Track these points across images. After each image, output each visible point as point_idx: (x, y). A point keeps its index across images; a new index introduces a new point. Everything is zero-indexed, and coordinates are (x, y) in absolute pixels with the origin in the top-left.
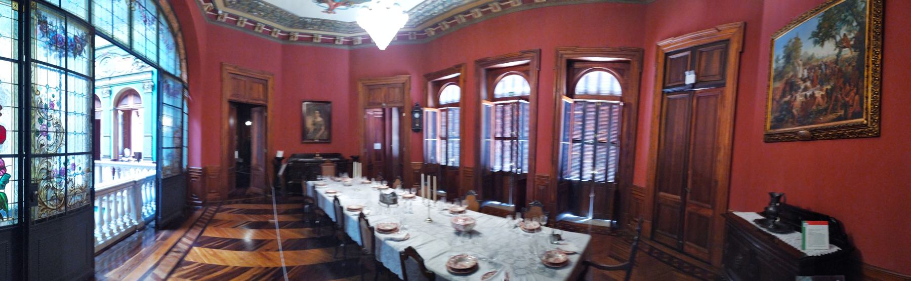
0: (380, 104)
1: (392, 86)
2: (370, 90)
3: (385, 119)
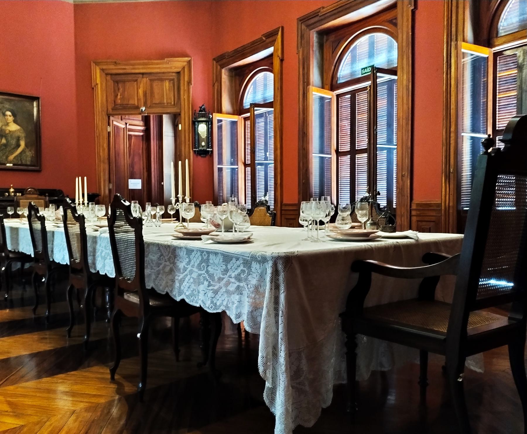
0: (138, 108)
1: (159, 77)
2: (117, 82)
3: (150, 137)
